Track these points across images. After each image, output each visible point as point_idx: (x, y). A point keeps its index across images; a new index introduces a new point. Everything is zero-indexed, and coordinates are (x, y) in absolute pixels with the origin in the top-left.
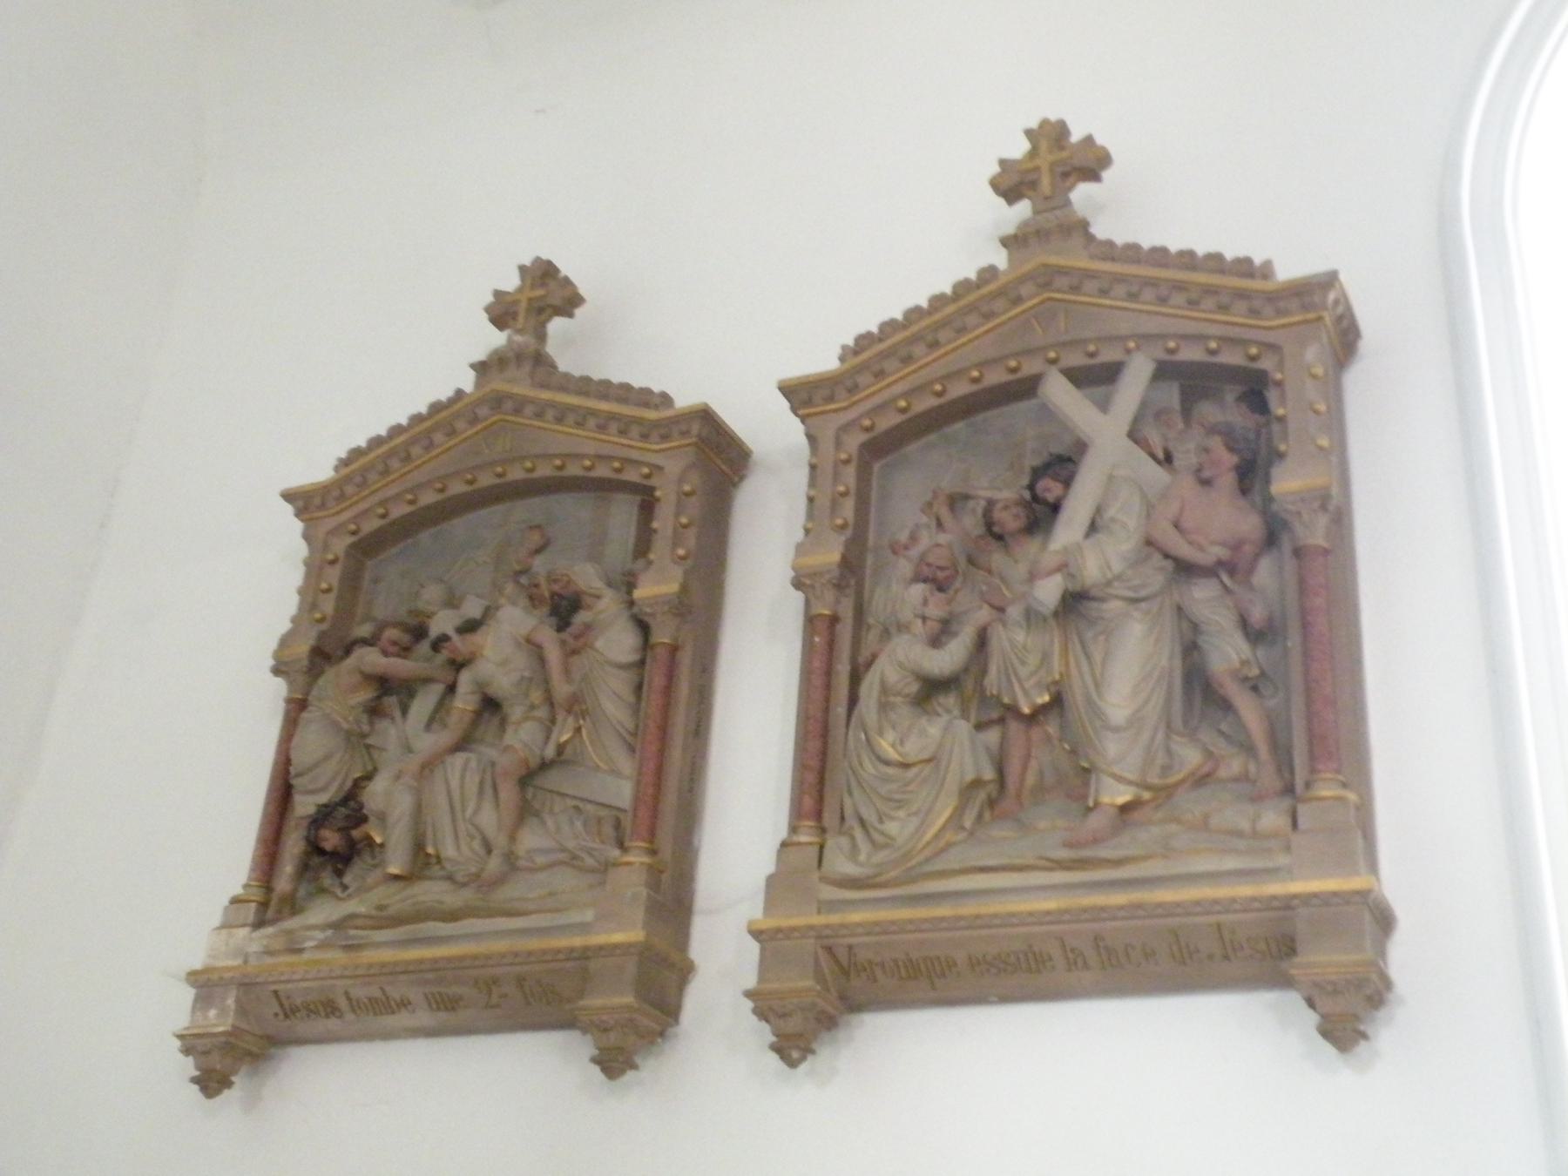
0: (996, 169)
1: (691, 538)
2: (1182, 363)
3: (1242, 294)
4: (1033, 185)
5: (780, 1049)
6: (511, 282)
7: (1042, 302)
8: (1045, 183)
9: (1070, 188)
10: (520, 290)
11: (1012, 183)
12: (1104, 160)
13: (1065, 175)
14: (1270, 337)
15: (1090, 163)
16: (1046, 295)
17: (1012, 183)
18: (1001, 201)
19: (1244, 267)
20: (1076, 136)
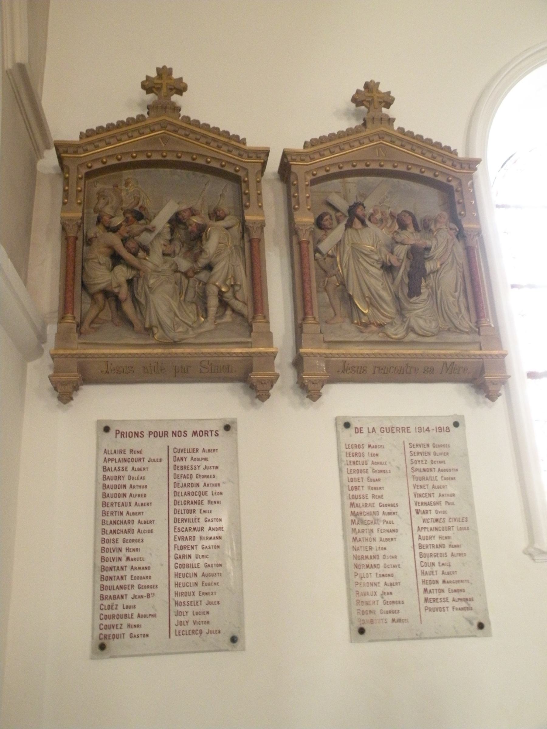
0: (144, 79)
1: (81, 195)
2: (197, 164)
3: (238, 148)
4: (159, 89)
5: (60, 398)
6: (382, 89)
7: (163, 133)
8: (164, 90)
9: (172, 95)
10: (379, 92)
11: (149, 86)
12: (185, 89)
13: (171, 89)
14: (457, 175)
15: (180, 88)
16: (382, 142)
17: (149, 86)
18: (144, 92)
19: (236, 138)
20: (175, 76)
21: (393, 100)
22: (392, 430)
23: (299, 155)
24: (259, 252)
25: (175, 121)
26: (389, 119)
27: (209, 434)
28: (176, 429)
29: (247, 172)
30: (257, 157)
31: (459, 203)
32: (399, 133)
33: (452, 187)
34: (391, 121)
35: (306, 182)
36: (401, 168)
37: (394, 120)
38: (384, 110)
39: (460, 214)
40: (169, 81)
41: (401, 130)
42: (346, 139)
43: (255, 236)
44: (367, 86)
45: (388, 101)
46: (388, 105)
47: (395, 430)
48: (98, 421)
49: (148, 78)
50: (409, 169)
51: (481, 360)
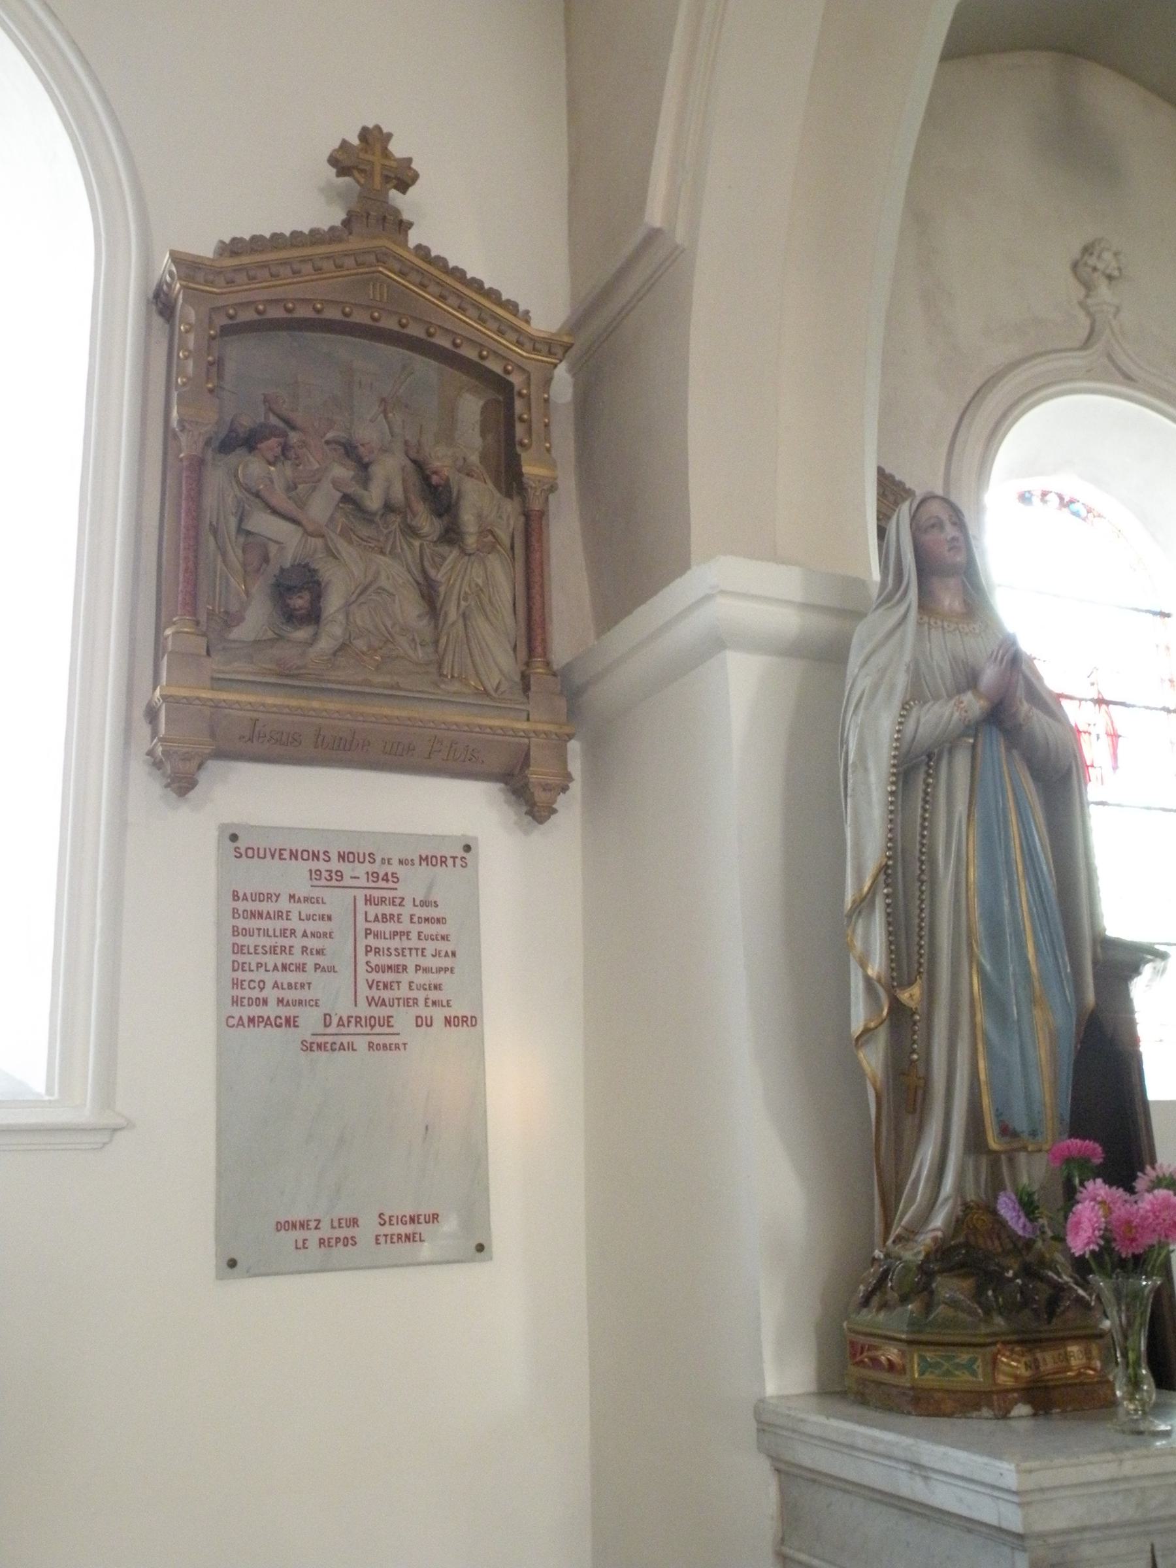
6: (397, 149)
21: (415, 177)
22: (281, 854)
23: (220, 273)
24: (540, 540)
25: (400, 251)
26: (401, 222)
27: (450, 862)
28: (344, 848)
29: (529, 378)
30: (534, 349)
31: (521, 420)
32: (417, 255)
33: (510, 385)
34: (404, 227)
35: (210, 328)
36: (415, 331)
37: (410, 225)
38: (393, 193)
39: (522, 444)
40: (386, 162)
41: (422, 251)
42: (308, 251)
43: (536, 506)
44: (365, 134)
45: (404, 178)
46: (403, 186)
47: (286, 854)
48: (476, 839)
49: (344, 144)
50: (430, 335)
51: (526, 740)
